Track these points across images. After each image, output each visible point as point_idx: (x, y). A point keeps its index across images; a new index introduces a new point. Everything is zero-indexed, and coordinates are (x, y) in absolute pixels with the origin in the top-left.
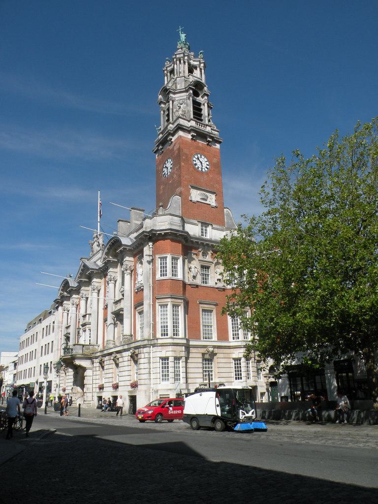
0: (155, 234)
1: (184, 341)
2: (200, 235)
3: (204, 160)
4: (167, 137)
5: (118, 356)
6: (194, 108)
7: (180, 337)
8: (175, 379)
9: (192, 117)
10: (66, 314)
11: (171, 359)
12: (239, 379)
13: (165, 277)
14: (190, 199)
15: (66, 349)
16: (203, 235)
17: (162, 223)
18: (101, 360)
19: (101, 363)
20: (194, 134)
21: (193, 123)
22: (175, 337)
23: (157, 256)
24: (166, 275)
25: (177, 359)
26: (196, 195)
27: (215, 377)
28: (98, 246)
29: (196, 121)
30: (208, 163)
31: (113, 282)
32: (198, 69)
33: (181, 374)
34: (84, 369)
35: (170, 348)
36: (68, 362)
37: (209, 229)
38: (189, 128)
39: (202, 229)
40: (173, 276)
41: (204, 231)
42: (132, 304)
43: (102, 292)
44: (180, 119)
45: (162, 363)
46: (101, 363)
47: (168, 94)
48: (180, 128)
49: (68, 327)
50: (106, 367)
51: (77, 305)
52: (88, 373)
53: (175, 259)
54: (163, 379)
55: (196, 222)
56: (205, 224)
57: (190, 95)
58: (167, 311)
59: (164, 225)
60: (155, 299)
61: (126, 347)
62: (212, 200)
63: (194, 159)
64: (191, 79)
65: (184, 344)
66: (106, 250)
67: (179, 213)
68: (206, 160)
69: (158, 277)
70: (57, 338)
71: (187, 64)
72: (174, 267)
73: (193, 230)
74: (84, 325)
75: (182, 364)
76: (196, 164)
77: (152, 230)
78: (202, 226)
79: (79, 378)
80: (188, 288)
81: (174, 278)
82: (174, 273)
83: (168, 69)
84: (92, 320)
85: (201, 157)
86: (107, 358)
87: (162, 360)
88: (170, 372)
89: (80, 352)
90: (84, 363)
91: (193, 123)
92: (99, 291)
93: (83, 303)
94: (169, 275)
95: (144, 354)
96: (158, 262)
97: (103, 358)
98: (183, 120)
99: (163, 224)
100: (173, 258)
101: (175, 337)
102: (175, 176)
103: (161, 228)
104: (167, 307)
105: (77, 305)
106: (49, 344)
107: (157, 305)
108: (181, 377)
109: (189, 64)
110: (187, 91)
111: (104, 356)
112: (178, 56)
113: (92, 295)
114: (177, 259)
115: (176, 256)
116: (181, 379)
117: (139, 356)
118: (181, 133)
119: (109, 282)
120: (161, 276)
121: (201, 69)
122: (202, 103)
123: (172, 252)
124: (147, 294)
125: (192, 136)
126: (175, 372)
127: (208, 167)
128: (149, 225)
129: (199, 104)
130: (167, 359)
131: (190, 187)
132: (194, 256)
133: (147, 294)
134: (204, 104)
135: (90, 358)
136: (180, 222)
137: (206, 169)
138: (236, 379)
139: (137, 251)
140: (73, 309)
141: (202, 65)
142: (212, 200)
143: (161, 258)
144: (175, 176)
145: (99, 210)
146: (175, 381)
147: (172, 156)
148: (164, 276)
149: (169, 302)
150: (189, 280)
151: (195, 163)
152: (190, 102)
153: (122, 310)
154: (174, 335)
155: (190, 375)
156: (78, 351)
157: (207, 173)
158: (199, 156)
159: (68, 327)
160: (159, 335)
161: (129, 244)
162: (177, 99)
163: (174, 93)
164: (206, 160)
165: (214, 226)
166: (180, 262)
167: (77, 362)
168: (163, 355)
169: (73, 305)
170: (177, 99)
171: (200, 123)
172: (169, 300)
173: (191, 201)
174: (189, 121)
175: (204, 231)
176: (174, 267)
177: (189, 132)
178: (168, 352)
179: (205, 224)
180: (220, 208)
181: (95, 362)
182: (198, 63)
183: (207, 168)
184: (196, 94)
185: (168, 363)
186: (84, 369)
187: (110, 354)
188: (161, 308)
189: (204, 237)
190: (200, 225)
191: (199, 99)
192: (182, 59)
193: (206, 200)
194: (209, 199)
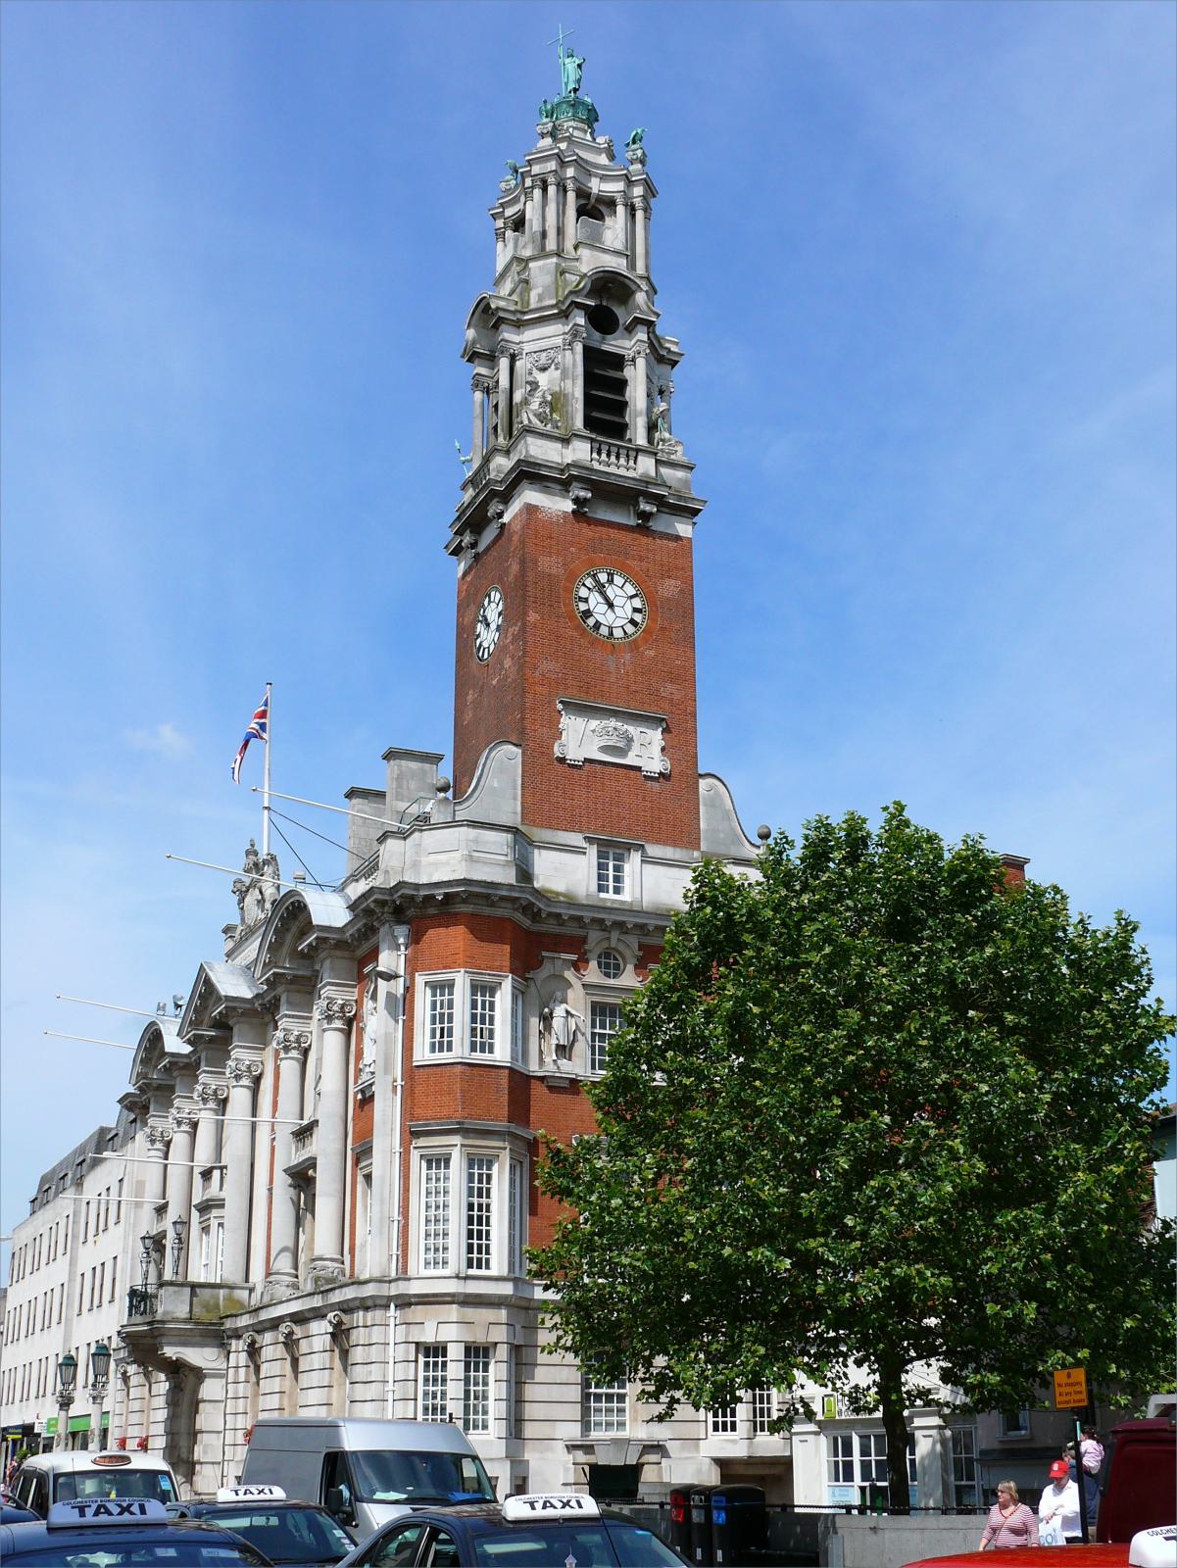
0: (412, 897)
1: (507, 1289)
2: (594, 887)
3: (621, 591)
4: (485, 503)
5: (298, 1331)
6: (591, 380)
7: (494, 1272)
8: (755, 1423)
9: (579, 422)
10: (295, 1066)
11: (455, 1352)
12: (725, 1429)
13: (445, 1054)
14: (557, 752)
15: (139, 1299)
16: (601, 888)
17: (439, 859)
18: (253, 1342)
19: (253, 1351)
20: (582, 494)
21: (580, 452)
22: (474, 1272)
23: (420, 980)
24: (450, 1049)
25: (478, 1355)
26: (581, 738)
27: (634, 1420)
28: (261, 902)
29: (592, 440)
30: (637, 603)
31: (294, 1054)
32: (620, 209)
33: (491, 1403)
34: (199, 1375)
35: (453, 1312)
36: (144, 1347)
37: (632, 864)
38: (562, 471)
39: (601, 867)
40: (473, 1049)
41: (611, 873)
42: (349, 1147)
43: (267, 1084)
44: (530, 439)
45: (427, 1364)
46: (253, 1351)
47: (496, 327)
48: (528, 474)
49: (303, 1134)
50: (357, 1354)
51: (349, 1022)
52: (210, 1389)
53: (483, 989)
54: (716, 1424)
55: (576, 839)
56: (612, 850)
57: (575, 334)
58: (446, 1178)
59: (447, 863)
60: (411, 1134)
61: (317, 1302)
62: (648, 751)
63: (583, 592)
64: (589, 262)
65: (506, 1297)
66: (271, 937)
67: (510, 811)
68: (631, 591)
69: (423, 1054)
70: (117, 1251)
71: (571, 196)
72: (481, 1021)
73: (566, 872)
74: (205, 1208)
75: (497, 1371)
76: (588, 614)
77: (401, 884)
78: (601, 855)
79: (185, 1407)
80: (538, 1091)
81: (479, 1057)
82: (481, 1038)
83: (509, 212)
84: (232, 1192)
85: (611, 581)
86: (268, 1337)
87: (427, 1356)
88: (448, 1397)
89: (182, 1311)
90: (198, 1356)
91: (580, 452)
92: (257, 1080)
93: (239, 1097)
94: (460, 1050)
95: (367, 1330)
96: (423, 999)
97: (258, 1338)
98: (540, 442)
99: (443, 857)
100: (475, 988)
101: (474, 1272)
102: (508, 663)
103: (435, 879)
104: (447, 1167)
105: (349, 1022)
106: (103, 1264)
107: (415, 1155)
108: (491, 1417)
109: (582, 194)
110: (564, 315)
111: (261, 1328)
112: (536, 169)
113: (321, 1039)
114: (492, 990)
115: (487, 978)
116: (491, 1423)
117: (354, 1334)
118: (530, 496)
119: (282, 1055)
120: (433, 1050)
121: (632, 210)
122: (629, 354)
123: (470, 963)
124: (388, 1112)
125: (576, 501)
126: (754, 1402)
127: (638, 617)
128: (395, 863)
129: (618, 361)
130: (434, 1351)
131: (560, 706)
132: (569, 975)
133: (388, 1112)
134: (633, 360)
135: (217, 1336)
136: (505, 850)
137: (630, 629)
138: (716, 1429)
139: (354, 950)
140: (329, 1045)
141: (638, 191)
142: (648, 751)
143: (434, 987)
144: (508, 663)
145: (267, 767)
146: (755, 1430)
147: (501, 580)
148: (441, 1050)
149: (455, 1147)
150: (541, 1061)
151: (583, 607)
152: (575, 359)
153: (312, 1163)
154: (470, 1265)
155: (530, 1411)
156: (173, 1306)
157: (634, 645)
158: (603, 577)
159: (303, 1134)
160: (416, 1266)
161: (340, 924)
162: (527, 348)
163: (519, 326)
164: (631, 591)
165: (653, 850)
166: (503, 999)
167: (170, 1352)
168: (428, 1336)
169: (153, 1142)
170: (527, 348)
171: (619, 447)
172: (457, 1140)
173: (562, 760)
174: (565, 441)
175: (611, 873)
176: (481, 1021)
177: (565, 485)
178: (446, 1328)
179: (612, 850)
180: (683, 776)
181: (233, 1349)
182: (620, 186)
183: (633, 622)
184: (603, 321)
185: (444, 1364)
186: (199, 1375)
187: (274, 1324)
188: (429, 1168)
189: (610, 895)
190: (593, 851)
191: (616, 344)
192: (551, 179)
193: (622, 752)
194: (636, 746)
